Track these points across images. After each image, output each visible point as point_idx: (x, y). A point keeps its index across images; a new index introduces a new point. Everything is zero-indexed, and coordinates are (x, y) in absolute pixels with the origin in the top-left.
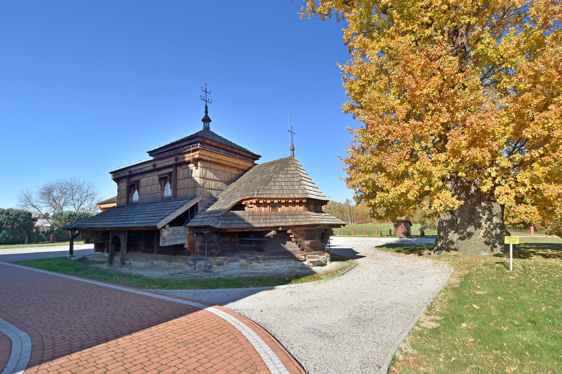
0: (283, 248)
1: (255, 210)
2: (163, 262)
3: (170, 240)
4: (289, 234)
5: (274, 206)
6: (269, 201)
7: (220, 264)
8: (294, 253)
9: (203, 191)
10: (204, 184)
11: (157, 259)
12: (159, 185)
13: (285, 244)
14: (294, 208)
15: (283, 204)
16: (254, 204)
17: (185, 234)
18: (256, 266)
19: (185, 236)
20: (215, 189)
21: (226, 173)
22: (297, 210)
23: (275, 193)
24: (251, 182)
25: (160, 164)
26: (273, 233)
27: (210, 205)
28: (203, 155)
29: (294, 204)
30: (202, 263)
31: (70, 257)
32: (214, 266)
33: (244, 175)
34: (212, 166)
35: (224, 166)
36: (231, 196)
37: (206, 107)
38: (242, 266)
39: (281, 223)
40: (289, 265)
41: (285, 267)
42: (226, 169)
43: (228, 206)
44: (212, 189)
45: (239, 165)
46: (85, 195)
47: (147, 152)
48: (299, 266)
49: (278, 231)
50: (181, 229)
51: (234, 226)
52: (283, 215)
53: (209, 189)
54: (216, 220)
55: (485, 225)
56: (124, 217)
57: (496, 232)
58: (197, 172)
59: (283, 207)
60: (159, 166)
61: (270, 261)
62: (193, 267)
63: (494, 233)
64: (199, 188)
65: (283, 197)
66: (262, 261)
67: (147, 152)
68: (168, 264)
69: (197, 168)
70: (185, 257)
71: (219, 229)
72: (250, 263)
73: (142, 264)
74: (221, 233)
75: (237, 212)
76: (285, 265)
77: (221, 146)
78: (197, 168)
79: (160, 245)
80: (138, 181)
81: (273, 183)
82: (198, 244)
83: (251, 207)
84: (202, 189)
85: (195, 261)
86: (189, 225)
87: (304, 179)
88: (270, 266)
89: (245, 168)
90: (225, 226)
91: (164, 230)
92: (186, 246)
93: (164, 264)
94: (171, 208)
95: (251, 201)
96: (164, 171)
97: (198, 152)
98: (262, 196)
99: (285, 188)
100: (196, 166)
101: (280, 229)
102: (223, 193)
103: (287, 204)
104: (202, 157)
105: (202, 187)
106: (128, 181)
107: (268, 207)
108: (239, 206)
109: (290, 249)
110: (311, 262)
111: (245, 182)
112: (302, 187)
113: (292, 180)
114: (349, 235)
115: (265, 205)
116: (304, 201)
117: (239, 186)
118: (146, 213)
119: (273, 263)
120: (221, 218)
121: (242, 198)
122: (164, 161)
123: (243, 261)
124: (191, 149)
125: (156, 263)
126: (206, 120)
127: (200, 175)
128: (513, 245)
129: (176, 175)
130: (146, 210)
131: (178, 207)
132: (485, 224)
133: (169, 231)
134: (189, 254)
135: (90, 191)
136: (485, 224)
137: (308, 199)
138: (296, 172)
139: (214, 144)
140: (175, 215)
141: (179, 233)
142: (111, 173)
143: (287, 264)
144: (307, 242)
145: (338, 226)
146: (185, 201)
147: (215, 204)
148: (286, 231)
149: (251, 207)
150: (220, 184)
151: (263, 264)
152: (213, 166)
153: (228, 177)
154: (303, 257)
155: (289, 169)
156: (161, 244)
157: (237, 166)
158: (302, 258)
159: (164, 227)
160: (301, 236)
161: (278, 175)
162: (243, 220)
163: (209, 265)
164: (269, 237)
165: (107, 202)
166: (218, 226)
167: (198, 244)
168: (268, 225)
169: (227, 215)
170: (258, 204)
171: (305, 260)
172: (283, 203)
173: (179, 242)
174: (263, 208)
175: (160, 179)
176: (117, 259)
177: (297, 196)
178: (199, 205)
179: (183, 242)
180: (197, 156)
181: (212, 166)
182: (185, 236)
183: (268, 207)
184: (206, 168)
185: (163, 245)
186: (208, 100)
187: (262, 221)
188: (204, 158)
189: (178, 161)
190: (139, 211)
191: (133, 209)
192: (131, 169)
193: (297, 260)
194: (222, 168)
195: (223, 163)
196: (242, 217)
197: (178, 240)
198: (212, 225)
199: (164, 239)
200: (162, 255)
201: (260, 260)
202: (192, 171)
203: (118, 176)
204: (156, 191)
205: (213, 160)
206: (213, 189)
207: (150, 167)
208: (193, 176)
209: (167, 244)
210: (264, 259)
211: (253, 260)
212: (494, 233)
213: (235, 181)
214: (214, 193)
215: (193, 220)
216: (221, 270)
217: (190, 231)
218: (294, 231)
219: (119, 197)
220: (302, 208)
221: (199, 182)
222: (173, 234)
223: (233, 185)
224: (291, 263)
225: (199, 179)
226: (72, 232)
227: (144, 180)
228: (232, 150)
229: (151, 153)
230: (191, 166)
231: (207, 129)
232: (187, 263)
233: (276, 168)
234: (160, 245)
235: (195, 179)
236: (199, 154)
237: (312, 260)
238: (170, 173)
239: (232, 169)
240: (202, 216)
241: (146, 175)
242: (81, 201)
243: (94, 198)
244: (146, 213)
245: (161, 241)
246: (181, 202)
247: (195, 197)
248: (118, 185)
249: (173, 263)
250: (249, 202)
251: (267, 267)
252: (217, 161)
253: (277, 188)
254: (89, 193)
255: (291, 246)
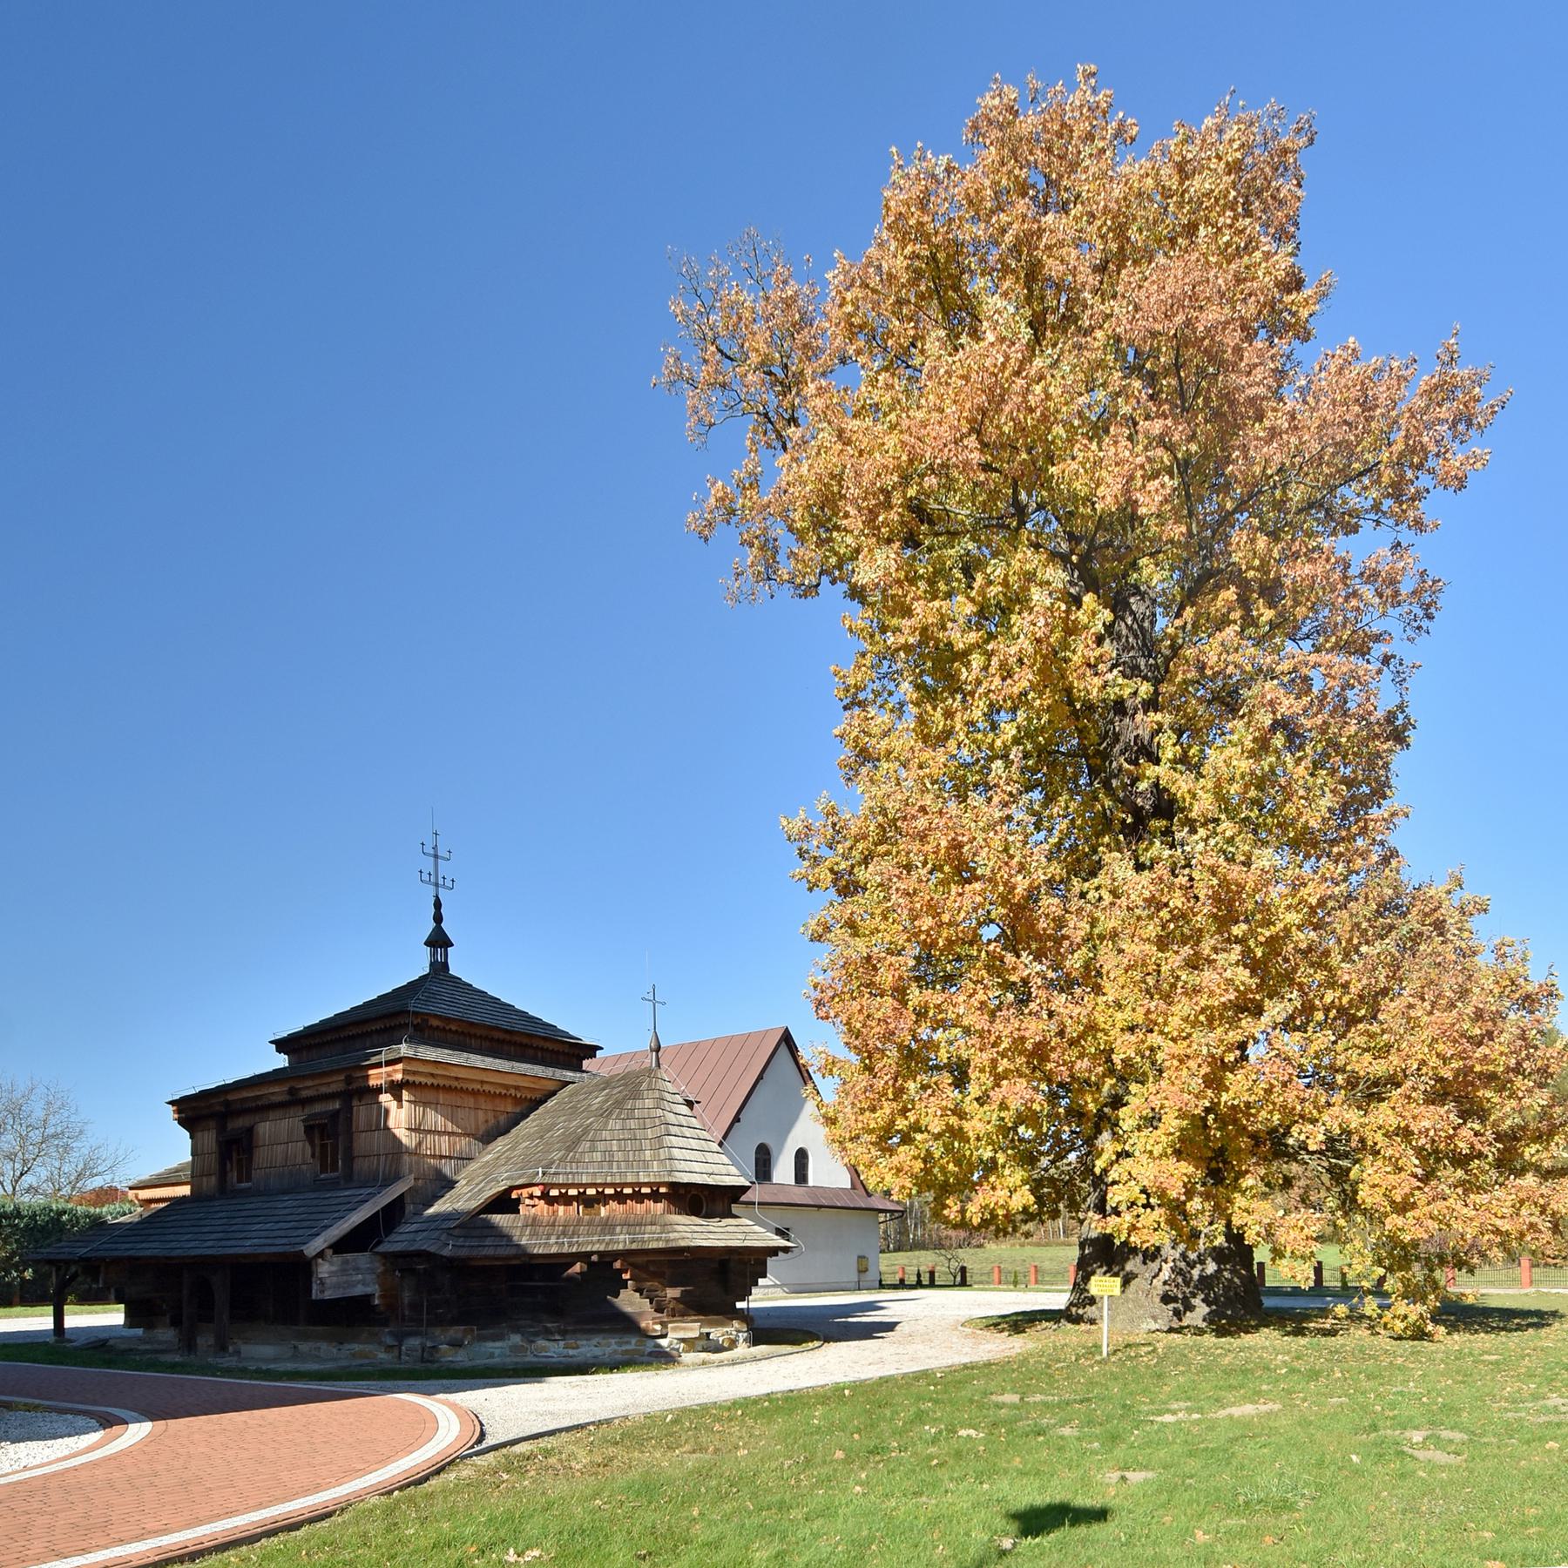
0: (612, 1305)
1: (542, 1212)
2: (324, 1346)
3: (337, 1286)
4: (621, 1271)
5: (589, 1202)
6: (573, 1192)
7: (456, 1344)
8: (637, 1318)
9: (418, 1163)
10: (419, 1144)
11: (306, 1337)
12: (307, 1144)
13: (617, 1296)
14: (639, 1208)
15: (647, 1196)
16: (539, 1198)
17: (372, 1271)
18: (544, 1349)
19: (374, 1276)
20: (450, 1158)
21: (481, 1113)
22: (648, 1211)
23: (589, 1172)
24: (541, 1137)
25: (308, 1089)
26: (577, 1268)
27: (436, 1197)
28: (414, 1073)
29: (638, 1197)
30: (414, 1342)
31: (56, 1341)
32: (444, 1347)
33: (532, 1116)
34: (441, 1096)
35: (475, 1093)
36: (488, 1178)
37: (438, 905)
38: (515, 1349)
39: (594, 1243)
40: (624, 1348)
41: (615, 1352)
42: (482, 1100)
43: (474, 1204)
44: (441, 1157)
45: (517, 1088)
46: (36, 1136)
47: (271, 1042)
48: (649, 1350)
49: (591, 1265)
50: (362, 1259)
51: (486, 1252)
52: (608, 1226)
53: (434, 1156)
54: (444, 1237)
55: (1172, 1252)
56: (220, 1229)
57: (1203, 1270)
58: (400, 1117)
59: (613, 1204)
60: (305, 1094)
61: (578, 1336)
62: (396, 1352)
63: (1196, 1273)
64: (406, 1158)
65: (609, 1180)
66: (557, 1337)
67: (271, 1042)
68: (335, 1351)
69: (400, 1106)
70: (377, 1329)
71: (450, 1260)
72: (533, 1342)
73: (267, 1351)
74: (459, 1268)
75: (497, 1219)
76: (615, 1347)
77: (473, 1031)
78: (400, 1106)
79: (314, 1297)
80: (250, 1131)
81: (588, 1144)
82: (407, 1296)
83: (533, 1206)
84: (414, 1158)
85: (400, 1338)
86: (381, 1249)
87: (673, 1130)
88: (577, 1348)
89: (538, 1096)
90: (463, 1253)
91: (320, 1261)
92: (377, 1302)
93: (325, 1348)
94: (339, 1207)
95: (530, 1190)
96: (318, 1108)
97: (400, 1066)
98: (555, 1180)
99: (619, 1156)
100: (399, 1099)
101: (594, 1258)
102: (473, 1166)
103: (620, 1198)
104: (411, 1078)
105: (414, 1153)
106: (221, 1129)
107: (575, 1204)
108: (505, 1203)
109: (628, 1309)
110: (683, 1340)
111: (529, 1137)
112: (663, 1154)
113: (639, 1134)
114: (1015, 1283)
115: (565, 1200)
116: (663, 1190)
117: (513, 1149)
118: (277, 1219)
119: (585, 1342)
120: (456, 1232)
121: (509, 1183)
122: (317, 1082)
123: (516, 1339)
124: (383, 1057)
125: (304, 1347)
126: (439, 941)
127: (410, 1122)
128: (1110, 1297)
129: (350, 1120)
130: (277, 1212)
131: (341, 1214)
132: (1173, 1248)
133: (331, 1264)
134: (385, 1323)
135: (52, 1120)
136: (1173, 1248)
137: (673, 1186)
138: (653, 1113)
139: (454, 1028)
140: (346, 1225)
141: (357, 1269)
142: (172, 1103)
143: (620, 1344)
144: (673, 1293)
145: (774, 1251)
146: (370, 1190)
147: (448, 1195)
148: (611, 1264)
149: (533, 1206)
150: (463, 1144)
151: (562, 1343)
152: (442, 1097)
153: (487, 1121)
154: (658, 1327)
155: (639, 1103)
156: (315, 1294)
157: (513, 1092)
158: (656, 1331)
159: (321, 1254)
160: (655, 1275)
161: (606, 1123)
162: (509, 1238)
163: (429, 1344)
164: (571, 1278)
165: (156, 1182)
166: (447, 1252)
167: (407, 1296)
168: (565, 1250)
169: (473, 1224)
170: (551, 1201)
171: (664, 1336)
172: (610, 1195)
173: (359, 1291)
174: (561, 1209)
175: (309, 1130)
176: (205, 1341)
177: (643, 1179)
178: (408, 1199)
179: (369, 1290)
180: (399, 1077)
181: (441, 1096)
182: (374, 1276)
183: (575, 1204)
184: (426, 1104)
185: (320, 1297)
186: (441, 881)
187: (553, 1241)
188: (418, 1079)
189: (354, 1086)
190: (258, 1212)
191: (239, 1207)
192: (231, 1097)
193: (644, 1334)
194: (470, 1101)
195: (471, 1086)
196: (506, 1231)
197: (354, 1286)
198: (432, 1249)
199: (322, 1284)
200: (320, 1328)
201: (552, 1333)
202: (387, 1111)
203: (192, 1111)
204: (299, 1160)
205: (442, 1082)
206: (446, 1157)
207: (278, 1092)
208: (391, 1123)
209: (328, 1295)
210: (564, 1333)
211: (537, 1334)
212: (1196, 1273)
213: (506, 1131)
214: (447, 1168)
215: (393, 1237)
216: (460, 1359)
217: (384, 1265)
218: (632, 1265)
219: (196, 1172)
220: (660, 1206)
221: (405, 1140)
222: (343, 1271)
223: (500, 1144)
224: (628, 1343)
225: (407, 1133)
226: (58, 1269)
227: (266, 1129)
228: (507, 1037)
229: (282, 1045)
230: (385, 1098)
231: (439, 968)
232: (380, 1343)
233: (607, 1101)
234: (314, 1297)
235: (396, 1132)
236: (405, 1072)
237: (682, 1335)
238: (335, 1115)
239: (498, 1101)
240: (414, 1227)
241: (272, 1115)
242: (25, 1162)
243: (67, 1149)
244: (277, 1219)
245: (315, 1287)
246: (361, 1191)
247: (396, 1177)
248: (191, 1137)
249: (347, 1346)
250: (525, 1192)
251: (571, 1352)
252: (455, 1084)
253: (598, 1156)
254: (50, 1131)
255: (630, 1301)
